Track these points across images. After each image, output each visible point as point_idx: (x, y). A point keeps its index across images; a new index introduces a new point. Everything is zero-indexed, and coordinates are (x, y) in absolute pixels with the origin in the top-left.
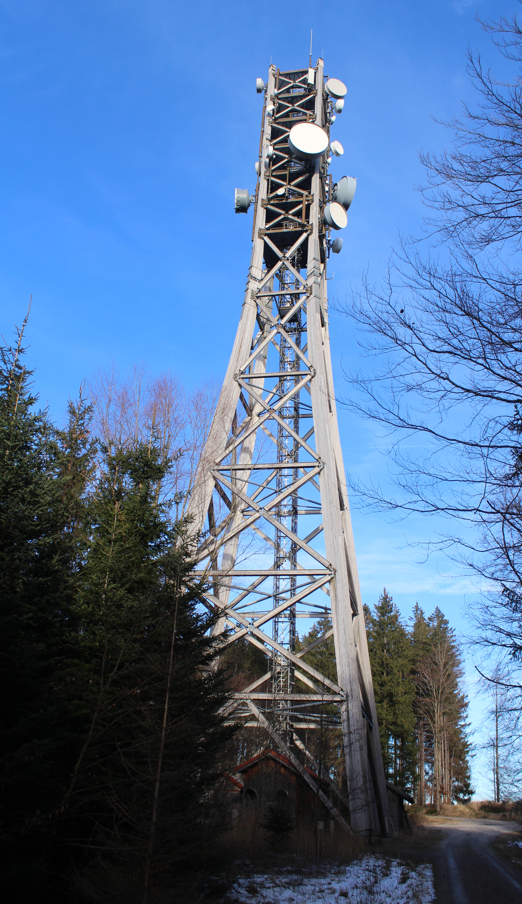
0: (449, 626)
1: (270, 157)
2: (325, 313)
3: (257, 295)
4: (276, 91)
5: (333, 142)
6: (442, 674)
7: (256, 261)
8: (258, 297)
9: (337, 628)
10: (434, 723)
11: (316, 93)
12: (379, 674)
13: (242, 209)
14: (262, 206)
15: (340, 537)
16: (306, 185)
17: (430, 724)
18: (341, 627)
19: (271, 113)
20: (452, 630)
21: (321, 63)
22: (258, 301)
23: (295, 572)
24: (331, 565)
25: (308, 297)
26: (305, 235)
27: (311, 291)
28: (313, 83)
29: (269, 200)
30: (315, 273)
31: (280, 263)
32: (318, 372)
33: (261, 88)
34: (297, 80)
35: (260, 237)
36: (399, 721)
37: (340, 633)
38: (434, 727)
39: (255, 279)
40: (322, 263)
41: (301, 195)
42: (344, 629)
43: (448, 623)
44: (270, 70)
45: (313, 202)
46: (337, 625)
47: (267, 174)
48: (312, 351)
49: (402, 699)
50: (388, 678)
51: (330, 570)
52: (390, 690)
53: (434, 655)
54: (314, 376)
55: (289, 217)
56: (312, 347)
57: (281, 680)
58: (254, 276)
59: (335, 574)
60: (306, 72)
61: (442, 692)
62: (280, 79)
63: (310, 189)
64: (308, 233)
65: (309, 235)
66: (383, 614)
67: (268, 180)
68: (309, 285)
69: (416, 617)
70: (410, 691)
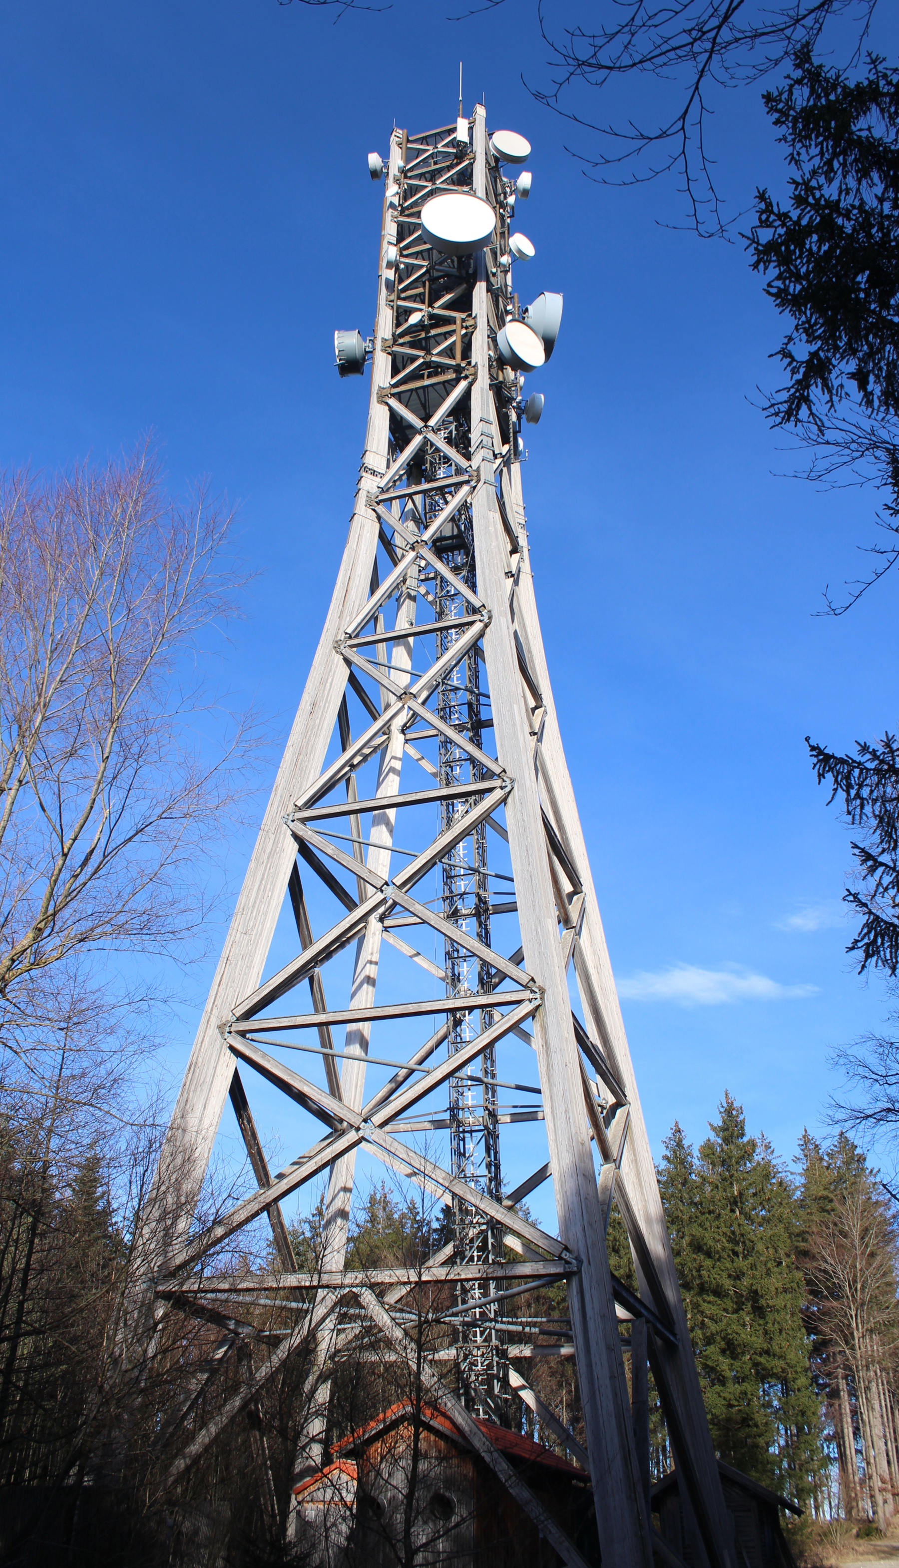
0: (868, 1164)
6: (859, 1252)
7: (375, 442)
8: (378, 503)
9: (552, 1112)
10: (853, 1348)
11: (474, 158)
12: (729, 1256)
13: (354, 366)
14: (384, 350)
15: (549, 920)
16: (464, 304)
17: (845, 1352)
18: (560, 1109)
19: (396, 201)
20: (874, 1172)
21: (481, 111)
23: (459, 1003)
24: (533, 980)
26: (463, 384)
27: (478, 476)
29: (395, 337)
30: (484, 442)
31: (417, 440)
32: (495, 614)
33: (378, 168)
34: (440, 142)
35: (382, 401)
36: (776, 1348)
37: (558, 1123)
38: (855, 1358)
39: (374, 473)
42: (566, 1112)
43: (865, 1159)
45: (475, 328)
46: (552, 1107)
48: (484, 579)
49: (779, 1302)
50: (747, 1262)
51: (533, 992)
52: (752, 1285)
53: (840, 1218)
54: (490, 623)
55: (433, 359)
57: (475, 1254)
58: (370, 467)
59: (542, 998)
60: (454, 130)
61: (863, 1287)
64: (469, 380)
66: (726, 1140)
67: (392, 307)
68: (474, 468)
69: (806, 1156)
70: (794, 1285)
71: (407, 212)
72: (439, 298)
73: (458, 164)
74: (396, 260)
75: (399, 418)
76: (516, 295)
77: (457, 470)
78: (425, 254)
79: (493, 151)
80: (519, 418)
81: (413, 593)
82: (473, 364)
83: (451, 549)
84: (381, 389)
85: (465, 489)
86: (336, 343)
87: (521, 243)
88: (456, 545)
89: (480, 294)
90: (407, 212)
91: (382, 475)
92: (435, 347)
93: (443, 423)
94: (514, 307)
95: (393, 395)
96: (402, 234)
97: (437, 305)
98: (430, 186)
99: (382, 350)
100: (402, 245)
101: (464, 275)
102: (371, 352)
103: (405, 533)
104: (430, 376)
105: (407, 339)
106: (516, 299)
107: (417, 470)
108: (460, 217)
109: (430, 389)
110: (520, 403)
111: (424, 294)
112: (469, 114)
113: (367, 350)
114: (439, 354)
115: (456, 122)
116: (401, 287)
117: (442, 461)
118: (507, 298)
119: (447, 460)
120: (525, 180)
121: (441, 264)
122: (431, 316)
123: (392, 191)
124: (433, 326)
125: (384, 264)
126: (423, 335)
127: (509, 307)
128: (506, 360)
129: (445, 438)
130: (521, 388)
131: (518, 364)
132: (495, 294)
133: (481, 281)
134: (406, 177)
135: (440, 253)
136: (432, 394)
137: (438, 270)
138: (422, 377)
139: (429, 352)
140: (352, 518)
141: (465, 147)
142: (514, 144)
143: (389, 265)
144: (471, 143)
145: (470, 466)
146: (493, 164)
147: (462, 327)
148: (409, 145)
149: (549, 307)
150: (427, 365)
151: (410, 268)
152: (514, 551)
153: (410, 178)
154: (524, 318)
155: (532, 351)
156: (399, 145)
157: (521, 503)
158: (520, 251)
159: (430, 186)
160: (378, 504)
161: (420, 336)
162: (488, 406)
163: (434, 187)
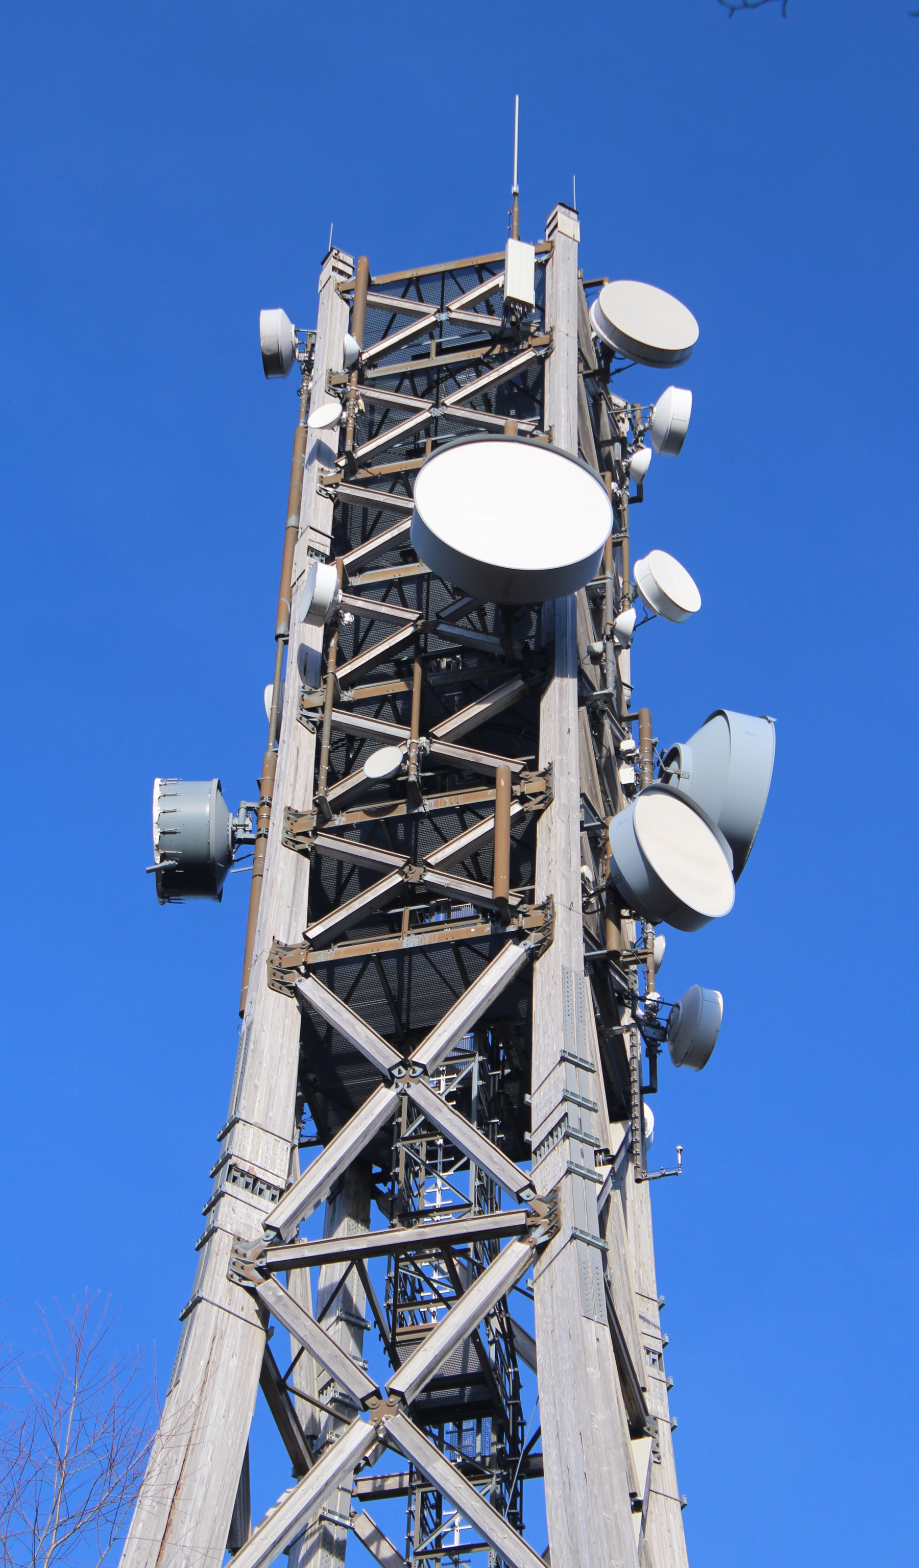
1: (326, 617)
2: (652, 1371)
3: (263, 1262)
4: (352, 344)
5: (643, 555)
8: (265, 1272)
11: (549, 347)
13: (195, 875)
14: (291, 842)
16: (515, 732)
19: (332, 440)
21: (568, 225)
22: (269, 1289)
25: (541, 1248)
26: (511, 956)
27: (554, 1214)
28: (531, 300)
30: (573, 1122)
31: (382, 1100)
33: (285, 350)
34: (454, 297)
35: (281, 982)
39: (254, 1184)
40: (613, 1118)
41: (488, 779)
44: (327, 271)
45: (548, 800)
47: (316, 700)
48: (571, 1519)
55: (430, 877)
56: (568, 1500)
58: (246, 1167)
60: (498, 266)
62: (370, 305)
63: (535, 750)
64: (530, 942)
65: (533, 955)
67: (319, 726)
68: (542, 1191)
71: (362, 474)
72: (449, 713)
73: (503, 359)
74: (334, 602)
75: (322, 1031)
76: (645, 714)
77: (482, 1190)
78: (409, 591)
79: (599, 331)
80: (652, 1052)
81: (338, 1533)
82: (540, 899)
83: (456, 1412)
84: (280, 948)
85: (515, 1252)
86: (156, 811)
87: (664, 574)
88: (484, 1404)
89: (560, 708)
90: (362, 474)
91: (280, 1193)
92: (434, 847)
93: (451, 1062)
94: (639, 744)
95: (312, 969)
96: (348, 527)
97: (442, 730)
98: (426, 411)
99: (285, 843)
100: (348, 559)
101: (519, 656)
102: (251, 842)
103: (329, 1357)
104: (418, 921)
105: (356, 816)
106: (646, 724)
107: (365, 1185)
108: (510, 503)
109: (418, 959)
110: (654, 1009)
111: (407, 696)
112: (536, 230)
113: (240, 835)
114: (445, 866)
115: (503, 247)
116: (341, 674)
117: (440, 1159)
118: (621, 719)
119: (454, 1153)
120: (675, 406)
121: (452, 619)
122: (428, 761)
123: (324, 413)
124: (430, 787)
125: (300, 609)
126: (402, 810)
127: (627, 745)
128: (630, 896)
129: (450, 1097)
130: (657, 967)
131: (661, 905)
132: (597, 709)
133: (563, 675)
134: (361, 381)
135: (456, 591)
136: (422, 972)
137: (443, 636)
138: (394, 926)
139: (414, 860)
140: (190, 1310)
141: (524, 315)
142: (656, 316)
143: (315, 613)
144: (541, 308)
145: (531, 1186)
146: (594, 365)
147: (513, 797)
148: (372, 298)
149: (739, 751)
150: (405, 894)
151: (364, 623)
152: (638, 1429)
153: (374, 383)
154: (666, 777)
155: (702, 878)
156: (345, 293)
157: (653, 1292)
158: (663, 598)
159: (426, 411)
160: (266, 1276)
161: (396, 816)
162: (581, 1020)
163: (437, 412)
